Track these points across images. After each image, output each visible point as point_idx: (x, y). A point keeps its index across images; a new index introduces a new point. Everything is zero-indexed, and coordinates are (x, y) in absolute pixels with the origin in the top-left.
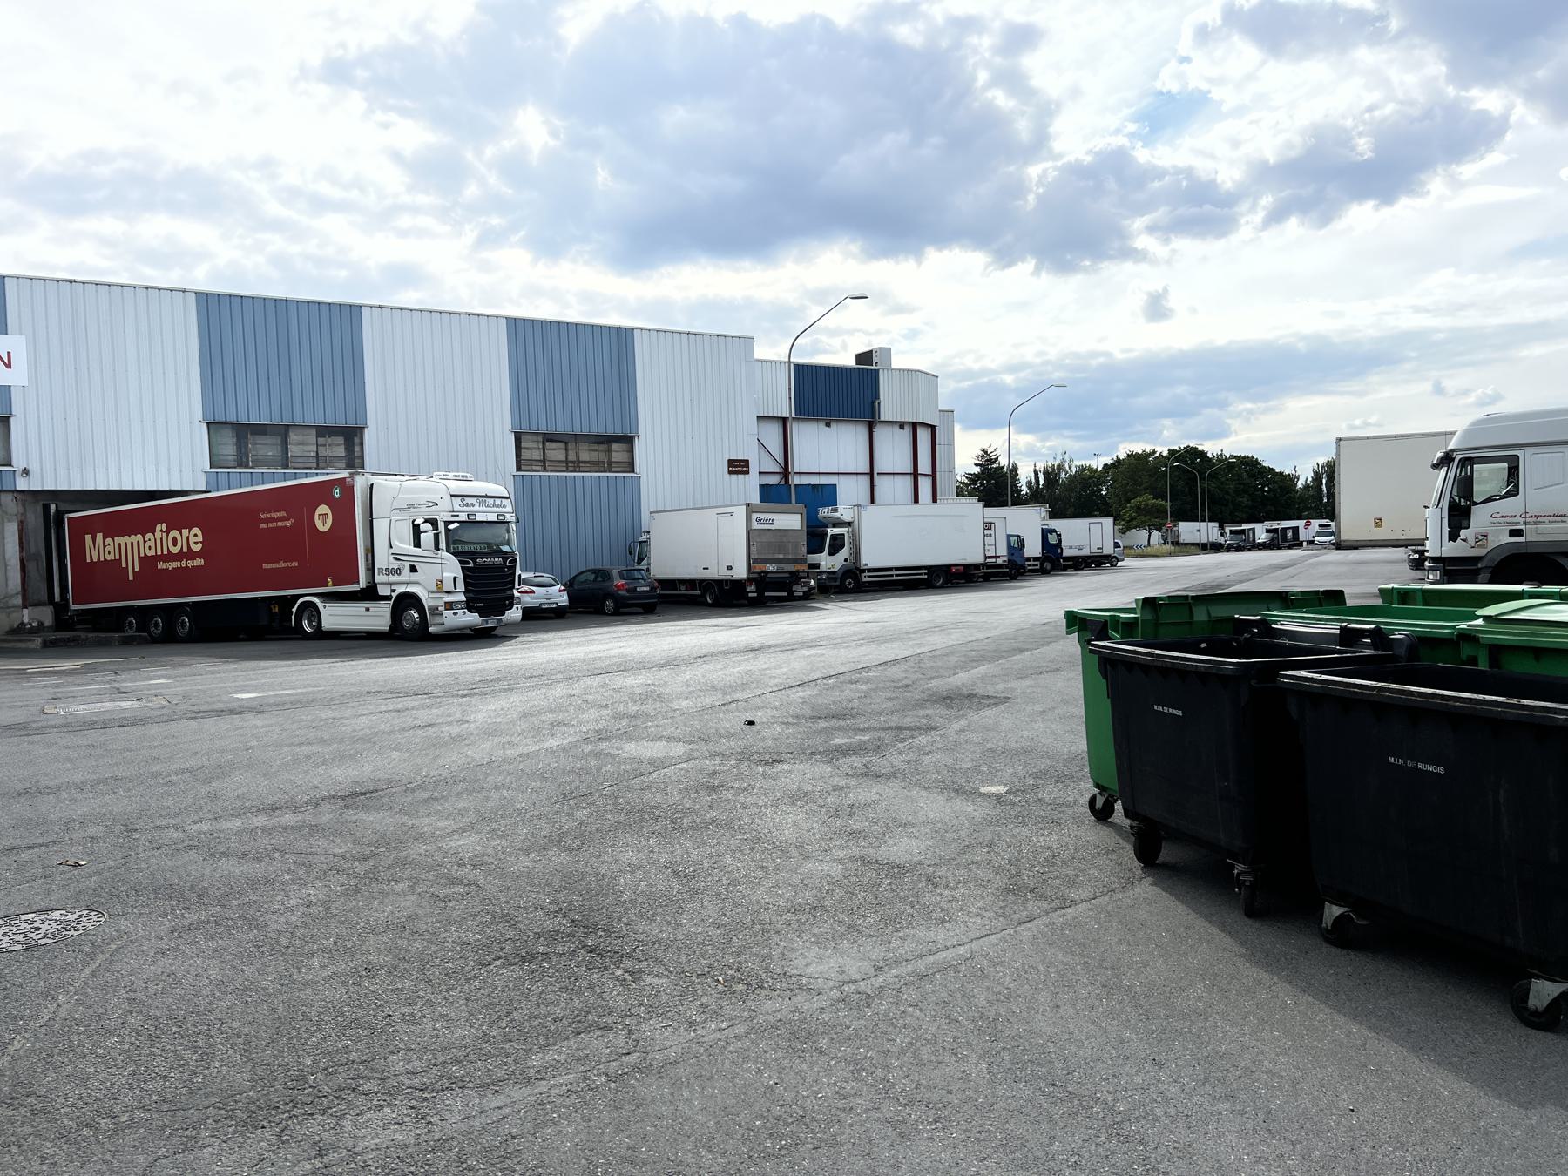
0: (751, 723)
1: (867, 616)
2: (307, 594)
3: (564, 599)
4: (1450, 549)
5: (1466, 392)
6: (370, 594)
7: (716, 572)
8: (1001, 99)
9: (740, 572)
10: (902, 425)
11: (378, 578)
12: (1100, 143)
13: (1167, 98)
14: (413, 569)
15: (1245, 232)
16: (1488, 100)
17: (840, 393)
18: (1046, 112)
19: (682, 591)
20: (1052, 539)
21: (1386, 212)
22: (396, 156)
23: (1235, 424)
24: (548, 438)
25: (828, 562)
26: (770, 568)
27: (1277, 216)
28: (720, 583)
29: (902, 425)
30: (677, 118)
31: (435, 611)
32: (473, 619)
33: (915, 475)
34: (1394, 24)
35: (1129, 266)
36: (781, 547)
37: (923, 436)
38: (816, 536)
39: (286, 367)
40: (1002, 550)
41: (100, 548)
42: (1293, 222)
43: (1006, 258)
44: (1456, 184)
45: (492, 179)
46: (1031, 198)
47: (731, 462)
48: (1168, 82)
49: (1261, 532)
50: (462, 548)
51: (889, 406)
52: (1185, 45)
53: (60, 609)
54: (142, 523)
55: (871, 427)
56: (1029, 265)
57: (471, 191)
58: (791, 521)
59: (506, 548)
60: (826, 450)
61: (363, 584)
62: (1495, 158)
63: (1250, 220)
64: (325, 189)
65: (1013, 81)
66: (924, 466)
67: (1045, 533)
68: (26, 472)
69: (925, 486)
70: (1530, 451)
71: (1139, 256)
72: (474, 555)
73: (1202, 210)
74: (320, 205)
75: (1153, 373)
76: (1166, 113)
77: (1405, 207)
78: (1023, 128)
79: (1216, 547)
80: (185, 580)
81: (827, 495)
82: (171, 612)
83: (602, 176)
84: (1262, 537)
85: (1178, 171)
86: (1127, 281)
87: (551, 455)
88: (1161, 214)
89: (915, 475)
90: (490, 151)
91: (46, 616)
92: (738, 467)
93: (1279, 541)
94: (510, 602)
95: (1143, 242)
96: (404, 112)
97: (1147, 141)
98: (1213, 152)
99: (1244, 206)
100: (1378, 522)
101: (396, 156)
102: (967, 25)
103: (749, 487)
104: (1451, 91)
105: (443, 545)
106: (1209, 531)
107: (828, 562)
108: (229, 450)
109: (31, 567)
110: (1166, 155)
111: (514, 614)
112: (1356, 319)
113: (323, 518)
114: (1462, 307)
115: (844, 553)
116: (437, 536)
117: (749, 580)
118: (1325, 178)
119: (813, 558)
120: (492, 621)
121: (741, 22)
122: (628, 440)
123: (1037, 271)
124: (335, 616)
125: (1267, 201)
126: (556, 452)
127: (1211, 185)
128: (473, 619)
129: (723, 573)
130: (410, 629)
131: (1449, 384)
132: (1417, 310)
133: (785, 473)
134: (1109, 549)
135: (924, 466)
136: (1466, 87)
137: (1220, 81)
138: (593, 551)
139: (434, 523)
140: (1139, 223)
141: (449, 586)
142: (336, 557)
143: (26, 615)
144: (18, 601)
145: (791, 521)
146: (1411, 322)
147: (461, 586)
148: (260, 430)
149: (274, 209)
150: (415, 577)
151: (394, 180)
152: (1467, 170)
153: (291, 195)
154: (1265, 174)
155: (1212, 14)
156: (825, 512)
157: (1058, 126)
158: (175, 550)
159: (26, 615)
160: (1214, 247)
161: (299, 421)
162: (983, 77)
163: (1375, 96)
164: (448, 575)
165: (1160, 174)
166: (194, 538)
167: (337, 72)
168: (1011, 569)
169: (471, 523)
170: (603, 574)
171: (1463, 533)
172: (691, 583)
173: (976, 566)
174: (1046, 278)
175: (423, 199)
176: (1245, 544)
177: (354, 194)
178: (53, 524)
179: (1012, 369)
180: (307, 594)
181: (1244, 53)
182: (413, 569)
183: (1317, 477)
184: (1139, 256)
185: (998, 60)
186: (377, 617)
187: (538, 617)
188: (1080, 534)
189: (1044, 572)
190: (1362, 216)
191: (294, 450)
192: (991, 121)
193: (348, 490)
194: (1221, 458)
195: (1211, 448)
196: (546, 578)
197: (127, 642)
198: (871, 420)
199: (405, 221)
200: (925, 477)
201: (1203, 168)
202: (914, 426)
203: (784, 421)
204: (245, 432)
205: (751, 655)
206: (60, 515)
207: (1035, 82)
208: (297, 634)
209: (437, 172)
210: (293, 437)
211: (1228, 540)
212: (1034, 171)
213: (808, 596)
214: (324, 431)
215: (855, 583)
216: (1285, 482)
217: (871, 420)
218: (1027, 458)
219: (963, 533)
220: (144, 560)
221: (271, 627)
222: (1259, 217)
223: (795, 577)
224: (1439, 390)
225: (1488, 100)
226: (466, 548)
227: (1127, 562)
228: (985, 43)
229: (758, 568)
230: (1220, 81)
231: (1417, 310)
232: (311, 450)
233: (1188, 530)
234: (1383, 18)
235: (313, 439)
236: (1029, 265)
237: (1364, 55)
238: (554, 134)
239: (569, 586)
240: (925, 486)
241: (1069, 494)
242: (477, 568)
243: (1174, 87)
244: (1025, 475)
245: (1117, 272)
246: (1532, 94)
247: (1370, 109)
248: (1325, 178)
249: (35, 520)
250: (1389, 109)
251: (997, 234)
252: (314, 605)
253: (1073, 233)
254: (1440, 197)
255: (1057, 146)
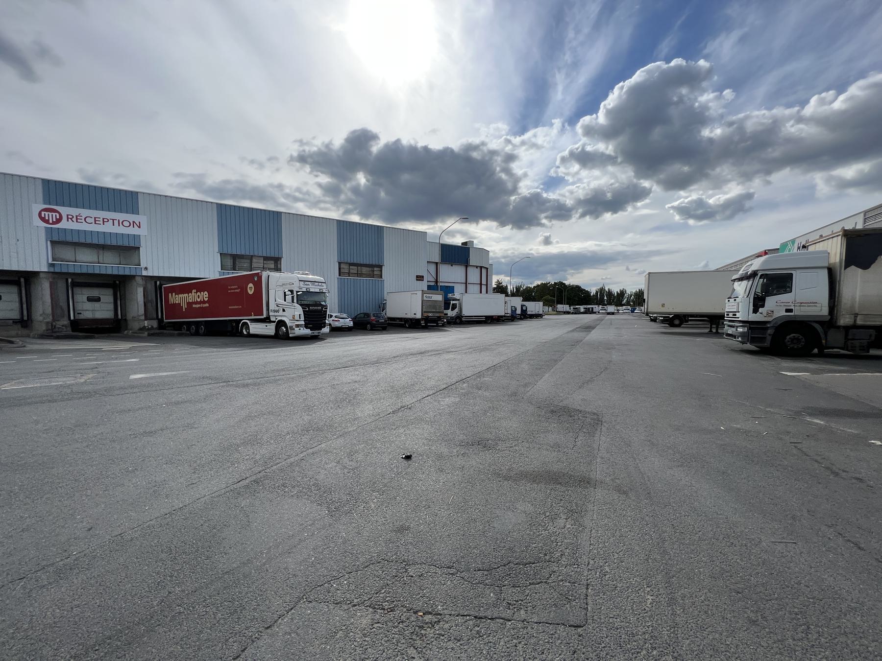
0: (408, 458)
1: (469, 335)
2: (245, 319)
3: (351, 324)
4: (753, 317)
5: (635, 270)
6: (267, 320)
7: (410, 316)
8: (503, 176)
9: (419, 316)
10: (477, 267)
11: (271, 314)
12: (533, 191)
13: (552, 178)
14: (284, 310)
15: (573, 220)
16: (646, 184)
17: (457, 255)
18: (517, 180)
19: (398, 322)
20: (524, 308)
21: (615, 216)
22: (320, 185)
23: (569, 277)
24: (351, 264)
25: (451, 313)
26: (430, 315)
27: (583, 215)
28: (411, 319)
29: (477, 267)
30: (405, 177)
31: (291, 328)
32: (308, 332)
33: (481, 284)
34: (619, 160)
35: (539, 228)
36: (434, 307)
37: (484, 271)
38: (447, 304)
39: (252, 232)
40: (509, 311)
41: (175, 299)
42: (588, 218)
43: (503, 224)
44: (636, 208)
45: (349, 194)
46: (511, 207)
47: (417, 276)
48: (552, 173)
49: (582, 308)
50: (303, 302)
51: (473, 261)
52: (558, 163)
53: (160, 321)
54: (187, 289)
55: (466, 267)
56: (510, 227)
57: (343, 197)
58: (439, 298)
59: (323, 303)
60: (451, 274)
61: (265, 316)
62: (647, 201)
63: (576, 216)
64: (297, 194)
65: (508, 171)
66: (484, 282)
67: (522, 306)
68: (146, 268)
69: (484, 288)
70: (798, 271)
71: (543, 225)
72: (308, 306)
73: (561, 212)
74: (297, 200)
75: (546, 261)
76: (553, 182)
77: (620, 215)
78: (510, 185)
79: (568, 313)
80: (202, 312)
81: (450, 289)
82: (197, 324)
83: (383, 194)
84: (582, 310)
85: (555, 200)
86: (540, 233)
87: (352, 271)
88: (549, 213)
89: (481, 284)
90: (348, 185)
91: (155, 324)
92: (420, 278)
93: (588, 312)
94: (324, 325)
95: (544, 221)
96: (322, 172)
97: (546, 191)
98: (565, 195)
99: (573, 212)
100: (663, 305)
101: (320, 185)
102: (493, 153)
103: (424, 285)
104: (635, 180)
105: (295, 301)
106: (566, 308)
107: (451, 313)
108: (229, 262)
109: (149, 305)
110: (552, 196)
111: (326, 330)
112: (606, 246)
113: (251, 289)
114: (635, 245)
115: (456, 310)
116: (293, 297)
117: (422, 319)
118: (597, 204)
119: (445, 311)
120: (316, 333)
121: (426, 148)
122: (380, 267)
123: (512, 229)
124: (256, 328)
125: (580, 211)
126: (354, 269)
127: (564, 205)
128: (308, 332)
129: (413, 316)
130: (282, 336)
131: (631, 267)
132: (623, 245)
133: (436, 282)
134: (541, 312)
135: (484, 282)
136: (639, 179)
137: (568, 174)
138: (365, 307)
139: (292, 291)
140: (543, 215)
141: (297, 318)
142: (255, 304)
143: (146, 323)
144: (143, 318)
145: (439, 298)
146: (621, 248)
147: (302, 318)
148: (241, 257)
149: (282, 200)
150: (284, 313)
151: (318, 192)
152: (639, 204)
153: (287, 196)
154: (580, 202)
155: (566, 153)
156: (450, 295)
157: (522, 184)
158: (199, 300)
159: (146, 323)
160: (565, 224)
161: (256, 254)
162: (498, 169)
163: (613, 181)
164: (297, 314)
165: (549, 201)
166: (205, 295)
167: (302, 159)
168: (512, 318)
169: (308, 293)
170: (367, 315)
171: (761, 310)
172: (401, 319)
173: (502, 317)
174: (515, 231)
175: (327, 199)
176: (577, 312)
177: (307, 197)
178: (158, 289)
179: (504, 257)
180: (245, 319)
181: (576, 167)
182: (284, 310)
183: (597, 292)
184: (543, 225)
185: (503, 164)
186: (269, 329)
187: (338, 331)
188: (534, 307)
189: (521, 319)
190: (608, 216)
191: (254, 265)
192: (501, 182)
193: (260, 278)
194: (570, 286)
195: (567, 283)
196: (345, 316)
197: (180, 335)
198: (466, 264)
199: (322, 205)
200: (484, 285)
201: (562, 199)
202: (481, 267)
203: (437, 263)
204: (235, 257)
205: (419, 357)
206: (161, 285)
207: (514, 172)
208: (241, 335)
209: (332, 191)
210: (254, 260)
211: (572, 310)
212: (513, 198)
213: (443, 326)
214: (266, 259)
215: (460, 321)
216: (587, 293)
217: (466, 264)
218: (510, 282)
219: (498, 305)
220: (189, 303)
221: (228, 332)
222: (578, 215)
223: (439, 318)
224: (628, 269)
225: (646, 184)
226: (305, 303)
227: (546, 317)
228: (499, 159)
229: (426, 315)
230: (568, 174)
231: (623, 245)
232: (261, 265)
233: (560, 307)
234: (616, 158)
235: (262, 261)
236: (510, 227)
237: (610, 168)
238: (367, 180)
239: (354, 320)
240: (484, 288)
241: (527, 294)
242: (310, 311)
243: (554, 175)
244: (510, 288)
245: (535, 229)
246: (659, 182)
247: (611, 184)
248: (597, 204)
249: (151, 287)
250: (617, 185)
251: (502, 217)
252: (247, 323)
253: (524, 216)
254: (630, 212)
255: (520, 191)
